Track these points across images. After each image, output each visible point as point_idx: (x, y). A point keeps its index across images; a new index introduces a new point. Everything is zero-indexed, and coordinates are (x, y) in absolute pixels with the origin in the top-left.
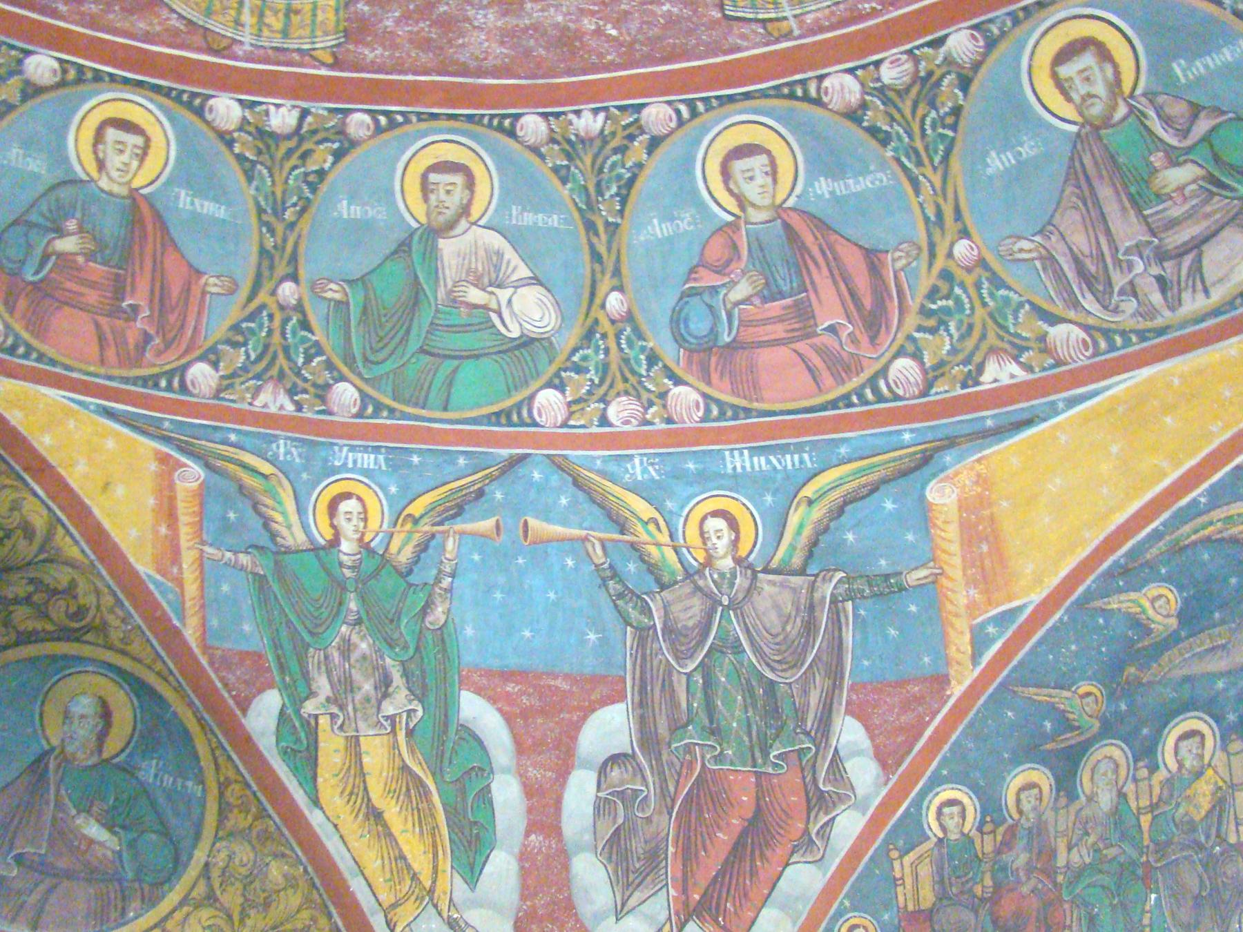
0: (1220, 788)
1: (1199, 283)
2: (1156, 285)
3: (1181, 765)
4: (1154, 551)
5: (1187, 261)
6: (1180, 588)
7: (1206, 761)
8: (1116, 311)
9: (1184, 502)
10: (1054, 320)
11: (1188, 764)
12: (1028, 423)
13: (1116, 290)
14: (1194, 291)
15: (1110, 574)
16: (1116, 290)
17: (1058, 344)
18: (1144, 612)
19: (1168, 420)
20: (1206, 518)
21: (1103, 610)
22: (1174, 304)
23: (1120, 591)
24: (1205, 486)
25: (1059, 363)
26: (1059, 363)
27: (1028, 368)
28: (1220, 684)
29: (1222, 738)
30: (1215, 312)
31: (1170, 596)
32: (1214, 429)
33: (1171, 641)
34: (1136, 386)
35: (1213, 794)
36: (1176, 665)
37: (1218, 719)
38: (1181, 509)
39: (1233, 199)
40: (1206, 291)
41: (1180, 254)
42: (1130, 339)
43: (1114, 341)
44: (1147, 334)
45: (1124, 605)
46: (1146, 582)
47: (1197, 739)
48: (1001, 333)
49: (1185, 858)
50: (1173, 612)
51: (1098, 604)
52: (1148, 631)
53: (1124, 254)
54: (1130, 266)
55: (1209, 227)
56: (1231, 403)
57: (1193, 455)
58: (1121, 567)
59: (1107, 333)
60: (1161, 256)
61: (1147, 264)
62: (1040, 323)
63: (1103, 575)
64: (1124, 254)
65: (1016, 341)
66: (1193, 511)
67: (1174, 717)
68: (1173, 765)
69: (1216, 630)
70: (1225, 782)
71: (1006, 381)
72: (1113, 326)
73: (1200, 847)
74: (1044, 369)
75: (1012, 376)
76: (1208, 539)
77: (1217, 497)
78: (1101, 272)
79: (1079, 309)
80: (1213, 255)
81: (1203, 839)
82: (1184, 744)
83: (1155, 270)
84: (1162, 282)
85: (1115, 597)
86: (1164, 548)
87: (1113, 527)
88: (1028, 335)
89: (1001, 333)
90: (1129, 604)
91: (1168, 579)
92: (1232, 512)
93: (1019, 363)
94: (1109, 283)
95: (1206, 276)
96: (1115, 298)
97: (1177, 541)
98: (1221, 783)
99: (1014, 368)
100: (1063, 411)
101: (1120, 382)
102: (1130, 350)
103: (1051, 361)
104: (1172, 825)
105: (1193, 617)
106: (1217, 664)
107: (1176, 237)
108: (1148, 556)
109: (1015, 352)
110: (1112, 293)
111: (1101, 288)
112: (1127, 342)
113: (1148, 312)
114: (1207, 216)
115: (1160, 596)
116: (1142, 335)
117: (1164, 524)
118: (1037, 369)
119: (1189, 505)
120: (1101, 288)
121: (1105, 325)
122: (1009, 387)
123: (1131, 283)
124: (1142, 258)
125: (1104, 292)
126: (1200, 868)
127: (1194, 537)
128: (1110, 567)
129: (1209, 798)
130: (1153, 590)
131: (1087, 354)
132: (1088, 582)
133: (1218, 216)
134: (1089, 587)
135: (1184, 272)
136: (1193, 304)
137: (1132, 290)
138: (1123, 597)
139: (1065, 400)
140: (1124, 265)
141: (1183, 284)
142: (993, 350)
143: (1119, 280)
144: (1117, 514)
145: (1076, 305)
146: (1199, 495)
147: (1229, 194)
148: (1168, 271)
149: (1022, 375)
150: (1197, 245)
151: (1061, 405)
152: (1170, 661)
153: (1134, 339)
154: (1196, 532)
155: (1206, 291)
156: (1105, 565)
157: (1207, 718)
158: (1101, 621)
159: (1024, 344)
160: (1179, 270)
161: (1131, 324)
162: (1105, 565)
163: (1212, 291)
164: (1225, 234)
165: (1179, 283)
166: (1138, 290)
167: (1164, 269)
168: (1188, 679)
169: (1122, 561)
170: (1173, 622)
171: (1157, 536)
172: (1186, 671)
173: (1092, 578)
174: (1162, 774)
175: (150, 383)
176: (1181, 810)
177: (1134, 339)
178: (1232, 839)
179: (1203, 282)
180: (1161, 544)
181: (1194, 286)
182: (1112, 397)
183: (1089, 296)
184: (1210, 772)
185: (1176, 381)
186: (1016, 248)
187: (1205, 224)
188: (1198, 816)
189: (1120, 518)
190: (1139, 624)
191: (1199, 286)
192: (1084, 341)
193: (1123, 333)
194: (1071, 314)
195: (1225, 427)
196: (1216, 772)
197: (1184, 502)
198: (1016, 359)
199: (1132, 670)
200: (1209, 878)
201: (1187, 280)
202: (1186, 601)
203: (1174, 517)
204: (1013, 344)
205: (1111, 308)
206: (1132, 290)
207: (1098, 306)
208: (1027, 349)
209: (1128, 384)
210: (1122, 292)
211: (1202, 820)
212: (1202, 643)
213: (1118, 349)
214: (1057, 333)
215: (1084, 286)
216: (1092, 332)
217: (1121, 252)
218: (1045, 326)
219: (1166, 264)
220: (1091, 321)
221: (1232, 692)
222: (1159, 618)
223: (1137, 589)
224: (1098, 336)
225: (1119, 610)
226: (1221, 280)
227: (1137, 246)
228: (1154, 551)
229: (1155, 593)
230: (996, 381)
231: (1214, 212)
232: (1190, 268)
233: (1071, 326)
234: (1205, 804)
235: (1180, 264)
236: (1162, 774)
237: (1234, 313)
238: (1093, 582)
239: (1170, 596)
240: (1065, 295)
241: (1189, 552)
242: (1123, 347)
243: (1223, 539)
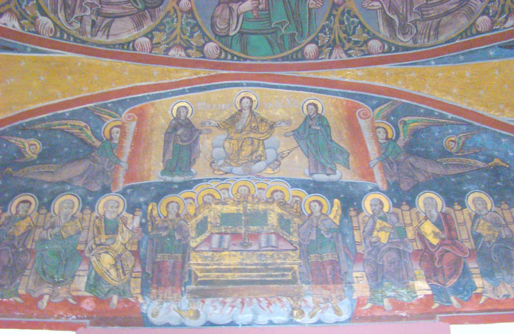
0: (31, 226)
1: (107, 31)
2: (91, 23)
3: (17, 212)
4: (39, 126)
5: (107, 21)
6: (44, 144)
7: (29, 214)
8: (70, 24)
9: (59, 112)
10: (44, 14)
11: (20, 213)
12: (11, 50)
13: (75, 16)
14: (104, 34)
15: (17, 128)
16: (75, 16)
17: (40, 24)
18: (25, 148)
19: (69, 78)
20: (65, 122)
21: (7, 140)
22: (94, 34)
23: (18, 136)
24: (71, 109)
25: (37, 32)
26: (37, 32)
27: (22, 27)
28: (46, 186)
29: (39, 207)
30: (107, 46)
31: (38, 146)
32: (85, 89)
33: (31, 163)
34: (64, 58)
35: (27, 227)
36: (31, 173)
37: (40, 199)
38: (57, 114)
39: (136, 8)
40: (108, 36)
41: (106, 16)
42: (70, 39)
43: (64, 36)
44: (78, 40)
45: (18, 143)
46: (30, 137)
47: (28, 204)
48: (18, 6)
49: (6, 250)
50: (37, 153)
51: (6, 138)
52: (24, 156)
53: (85, 4)
54: (85, 10)
55: (121, 13)
56: (95, 83)
57: (72, 95)
58: (24, 127)
59: (62, 31)
60: (99, 13)
61: (92, 13)
62: (37, 11)
63: (14, 127)
64: (85, 4)
65: (24, 14)
66: (61, 117)
67: (21, 193)
68: (14, 211)
69: (52, 165)
70: (33, 223)
71: (10, 27)
72: (66, 30)
73: (14, 247)
74: (29, 31)
75: (14, 27)
76: (62, 130)
77: (74, 115)
78: (72, 6)
79: (56, 15)
80: (118, 24)
81: (16, 244)
82: (22, 205)
83: (93, 17)
84: (94, 23)
85: (15, 138)
86: (44, 126)
87: (26, 109)
88: (30, 14)
89: (18, 6)
90: (20, 143)
91: (40, 139)
92: (77, 124)
93: (20, 23)
94: (73, 12)
95: (111, 31)
96: (73, 19)
97: (50, 126)
98: (32, 224)
99: (17, 24)
100: (29, 53)
101: (58, 53)
102: (67, 42)
103: (34, 30)
104: (4, 235)
105: (44, 157)
106: (48, 178)
107: (108, 9)
108: (36, 127)
109: (20, 17)
110: (72, 17)
111: (69, 12)
112: (232, 59)
113: (82, 32)
114: (123, 8)
115: (34, 145)
116: (76, 39)
117: (48, 117)
118: (26, 30)
119: (61, 114)
120: (69, 12)
121: (63, 28)
122: (10, 30)
123: (82, 17)
124: (91, 9)
125: (69, 15)
126: (11, 255)
127: (57, 127)
128: (18, 125)
129: (25, 228)
130: (33, 141)
131: (50, 35)
132: (6, 127)
133: (127, 11)
134: (6, 129)
135: (104, 24)
136: (101, 38)
137: (81, 20)
138: (19, 139)
139: (32, 48)
140: (83, 8)
141: (101, 29)
142: (10, 10)
143: (78, 13)
144: (31, 105)
145: (56, 13)
146: (67, 112)
147: (136, 6)
148: (98, 20)
149: (18, 28)
150: (115, 17)
151: (29, 50)
152: (28, 170)
153: (72, 39)
154: (59, 125)
155: (108, 36)
156: (16, 124)
157: (35, 197)
158: (5, 145)
159: (26, 16)
160: (102, 23)
161: (74, 33)
162: (16, 124)
163: (110, 37)
164: (126, 19)
165: (100, 27)
166: (83, 21)
167: (97, 19)
168: (33, 180)
169: (25, 124)
170: (35, 157)
171: (43, 120)
172: (34, 177)
173: (9, 126)
174: (8, 214)
175: (464, 35)
176: (11, 231)
177: (72, 39)
178: (29, 247)
179: (109, 32)
180: (43, 124)
181: (105, 31)
182: (52, 57)
183: (63, 12)
184: (29, 218)
185: (80, 64)
186: (371, 5)
187: (121, 11)
188: (17, 234)
189: (32, 107)
190: (20, 152)
191: (106, 33)
192: (51, 29)
193: (69, 35)
194: (52, 16)
195: (89, 91)
196: (31, 219)
197: (59, 112)
198: (19, 21)
199: (10, 169)
200: (14, 260)
201: (104, 28)
202: (44, 150)
203: (53, 116)
204: (21, 14)
205: (69, 22)
206: (81, 20)
207: (64, 18)
208: (26, 19)
209: (61, 55)
210: (76, 18)
211: (19, 236)
212: (44, 168)
213: (63, 40)
214: (43, 20)
215: (63, 8)
216: (57, 27)
217: (85, 2)
218: (38, 14)
219: (99, 18)
220: (58, 23)
221: (50, 191)
222: (29, 153)
223: (25, 138)
224: (58, 29)
225: (14, 143)
226: (115, 35)
227: (91, 4)
228: (39, 126)
229: (33, 142)
230: (5, 24)
231: (125, 9)
232: (107, 23)
233: (49, 20)
234: (22, 230)
235: (104, 20)
236: (8, 214)
237: (113, 50)
238: (9, 128)
239: (38, 146)
240: (53, 6)
241: (53, 132)
242: (65, 40)
243: (68, 132)
